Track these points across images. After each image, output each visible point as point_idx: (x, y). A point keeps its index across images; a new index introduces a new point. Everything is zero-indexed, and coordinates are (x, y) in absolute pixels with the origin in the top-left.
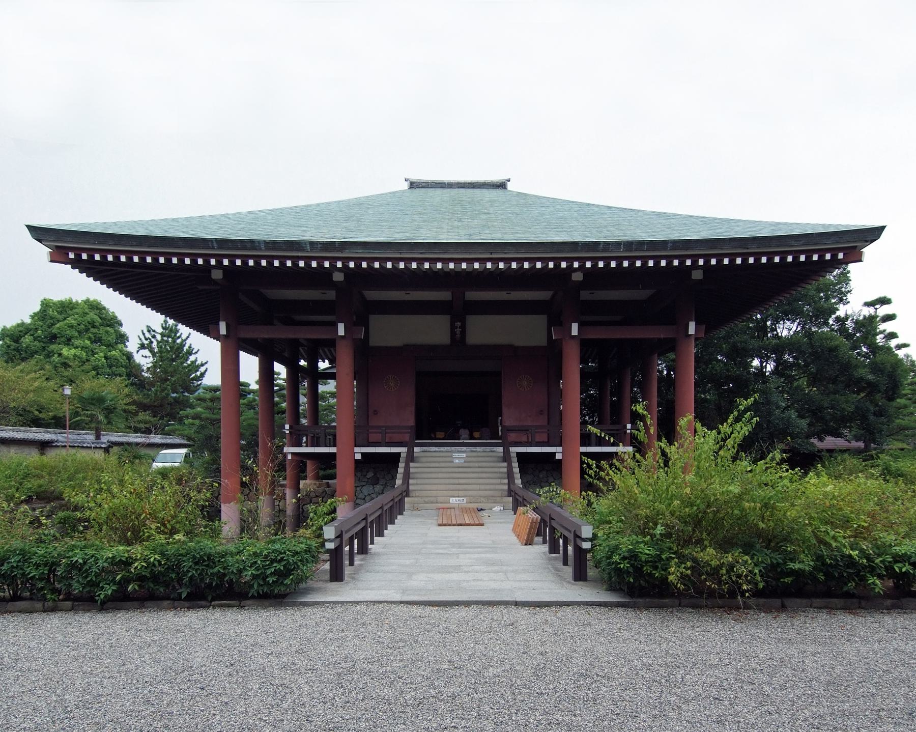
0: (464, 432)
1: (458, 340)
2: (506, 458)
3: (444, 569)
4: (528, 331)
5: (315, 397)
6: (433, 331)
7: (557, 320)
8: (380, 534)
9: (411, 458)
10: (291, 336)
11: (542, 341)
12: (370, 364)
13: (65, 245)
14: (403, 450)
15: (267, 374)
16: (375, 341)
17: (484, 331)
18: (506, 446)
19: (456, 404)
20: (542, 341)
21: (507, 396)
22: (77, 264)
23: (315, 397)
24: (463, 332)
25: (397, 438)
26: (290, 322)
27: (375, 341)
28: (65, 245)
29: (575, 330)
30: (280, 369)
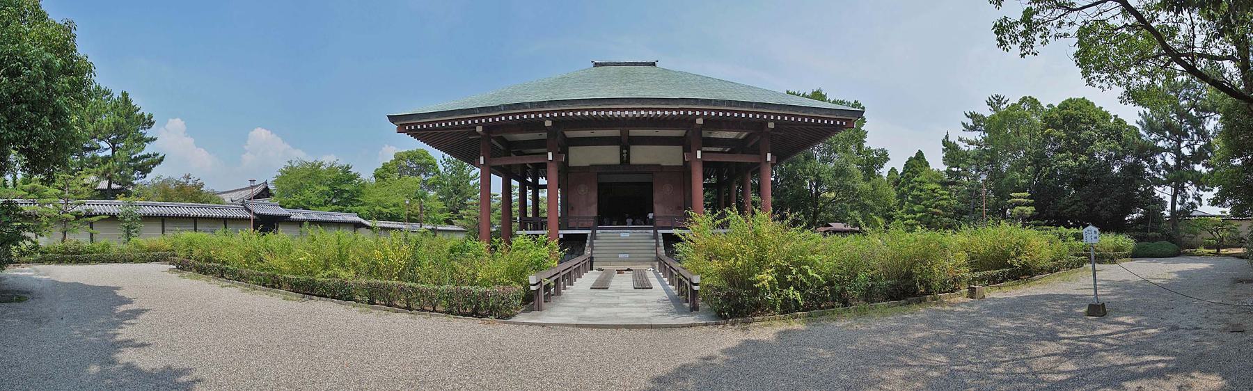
0: (629, 221)
1: (625, 160)
2: (655, 237)
3: (609, 305)
4: (670, 156)
5: (536, 200)
6: (609, 156)
7: (688, 149)
8: (571, 284)
9: (594, 237)
10: (520, 162)
11: (680, 163)
12: (568, 178)
13: (405, 124)
14: (589, 232)
15: (507, 189)
16: (572, 163)
17: (641, 155)
18: (655, 229)
19: (626, 200)
20: (680, 163)
21: (657, 197)
22: (410, 132)
23: (536, 200)
24: (628, 157)
25: (586, 224)
26: (520, 154)
27: (572, 163)
28: (405, 124)
29: (699, 156)
30: (515, 183)
